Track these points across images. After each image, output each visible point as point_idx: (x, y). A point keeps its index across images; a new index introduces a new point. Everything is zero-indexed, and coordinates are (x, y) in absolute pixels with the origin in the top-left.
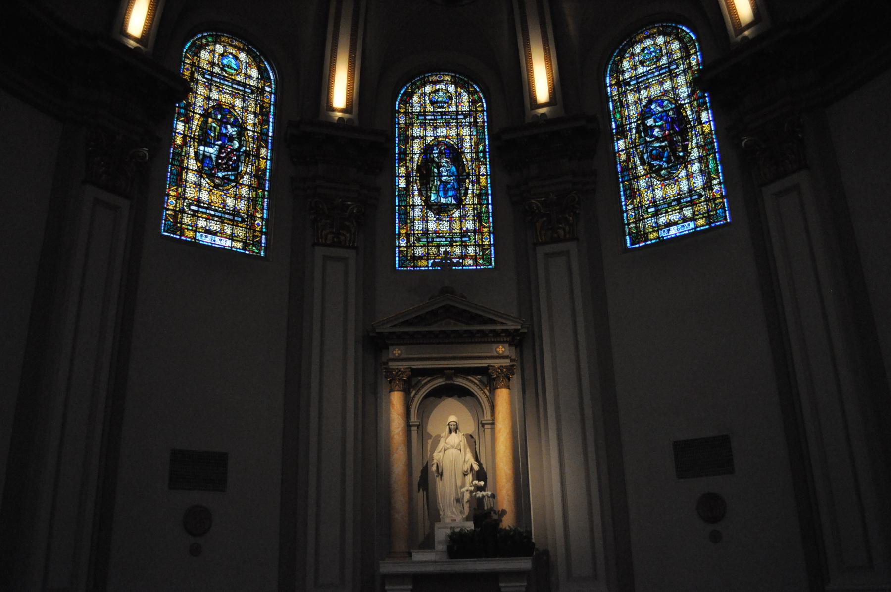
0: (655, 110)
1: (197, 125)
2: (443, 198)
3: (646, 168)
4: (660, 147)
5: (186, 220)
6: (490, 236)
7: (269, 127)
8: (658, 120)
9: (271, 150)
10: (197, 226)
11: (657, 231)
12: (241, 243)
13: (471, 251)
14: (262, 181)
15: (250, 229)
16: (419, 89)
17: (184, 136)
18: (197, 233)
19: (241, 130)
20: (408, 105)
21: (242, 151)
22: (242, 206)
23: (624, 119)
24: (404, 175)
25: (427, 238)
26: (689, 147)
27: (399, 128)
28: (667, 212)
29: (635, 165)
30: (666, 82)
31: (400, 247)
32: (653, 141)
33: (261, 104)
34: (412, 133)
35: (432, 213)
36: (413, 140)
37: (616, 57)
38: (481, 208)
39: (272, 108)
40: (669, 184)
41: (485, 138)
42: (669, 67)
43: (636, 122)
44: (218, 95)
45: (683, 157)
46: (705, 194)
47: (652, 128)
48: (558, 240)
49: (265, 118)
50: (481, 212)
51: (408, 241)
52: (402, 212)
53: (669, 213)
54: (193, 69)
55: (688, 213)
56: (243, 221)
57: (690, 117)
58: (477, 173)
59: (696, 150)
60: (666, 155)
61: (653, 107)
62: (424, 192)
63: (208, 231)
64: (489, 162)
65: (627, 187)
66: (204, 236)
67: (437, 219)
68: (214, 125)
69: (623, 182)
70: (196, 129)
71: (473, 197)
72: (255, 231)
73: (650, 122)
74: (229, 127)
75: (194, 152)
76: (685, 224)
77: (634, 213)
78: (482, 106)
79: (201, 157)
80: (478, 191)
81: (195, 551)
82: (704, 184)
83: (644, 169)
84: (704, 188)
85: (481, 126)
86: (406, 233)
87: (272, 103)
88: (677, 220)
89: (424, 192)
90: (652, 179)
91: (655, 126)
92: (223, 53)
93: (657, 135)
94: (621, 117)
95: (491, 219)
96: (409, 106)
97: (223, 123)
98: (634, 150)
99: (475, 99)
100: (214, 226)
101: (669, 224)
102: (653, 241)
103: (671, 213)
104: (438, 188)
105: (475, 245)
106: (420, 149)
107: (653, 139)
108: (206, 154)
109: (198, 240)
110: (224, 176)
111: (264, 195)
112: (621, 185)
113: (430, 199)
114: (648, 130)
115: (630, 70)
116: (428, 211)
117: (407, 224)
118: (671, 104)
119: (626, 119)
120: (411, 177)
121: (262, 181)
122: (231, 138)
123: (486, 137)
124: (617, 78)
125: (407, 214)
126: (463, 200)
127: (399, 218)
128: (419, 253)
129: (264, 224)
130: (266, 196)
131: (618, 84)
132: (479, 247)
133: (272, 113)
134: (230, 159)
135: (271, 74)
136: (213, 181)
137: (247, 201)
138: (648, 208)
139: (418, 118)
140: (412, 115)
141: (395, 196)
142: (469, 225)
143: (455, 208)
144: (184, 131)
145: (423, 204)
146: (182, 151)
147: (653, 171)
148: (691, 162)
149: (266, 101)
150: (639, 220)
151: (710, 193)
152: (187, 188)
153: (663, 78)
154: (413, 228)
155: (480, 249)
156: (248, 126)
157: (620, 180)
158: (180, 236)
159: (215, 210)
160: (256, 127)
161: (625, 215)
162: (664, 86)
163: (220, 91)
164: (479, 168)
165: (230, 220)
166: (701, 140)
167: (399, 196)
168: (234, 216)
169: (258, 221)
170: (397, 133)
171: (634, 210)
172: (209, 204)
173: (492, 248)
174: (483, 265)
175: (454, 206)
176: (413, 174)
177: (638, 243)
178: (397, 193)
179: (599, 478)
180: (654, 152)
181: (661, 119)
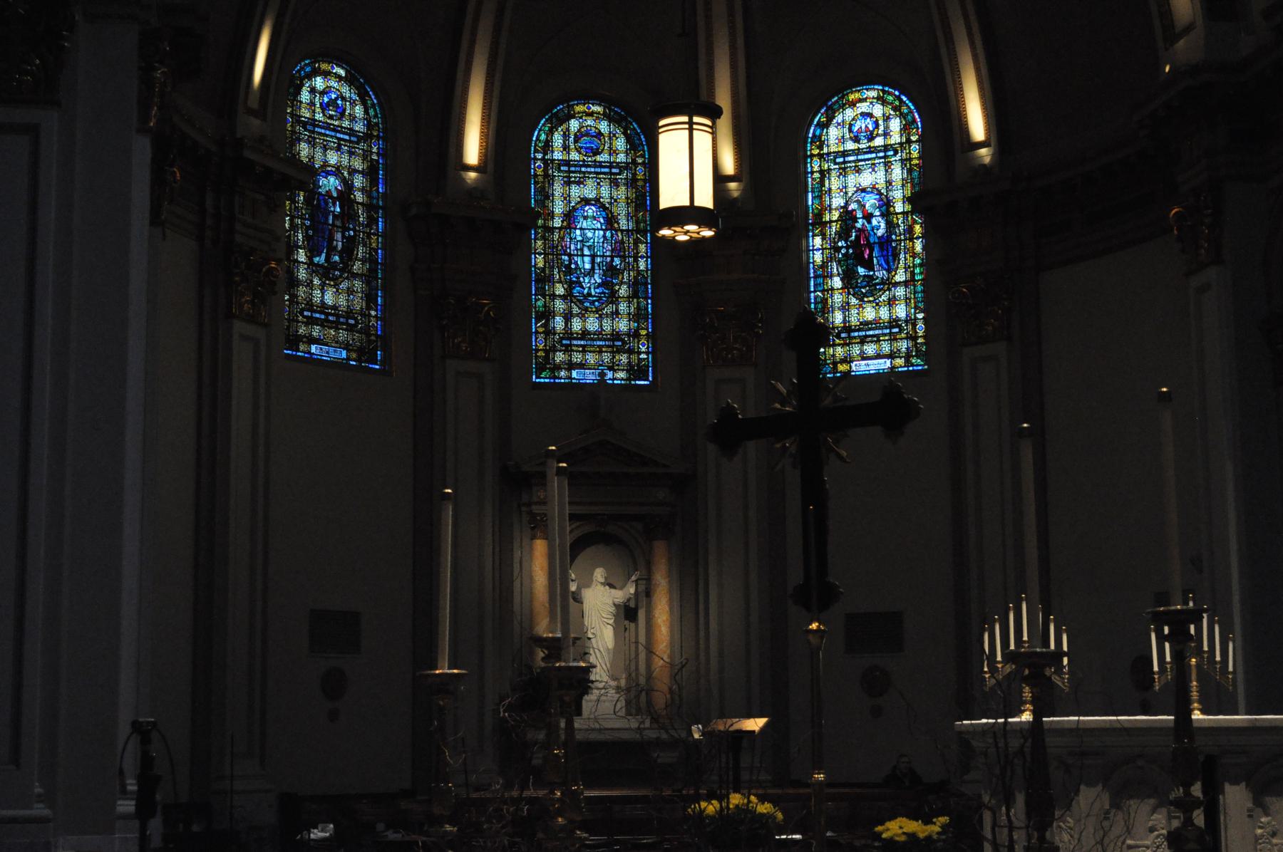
81: (334, 685)
165: (608, 346)
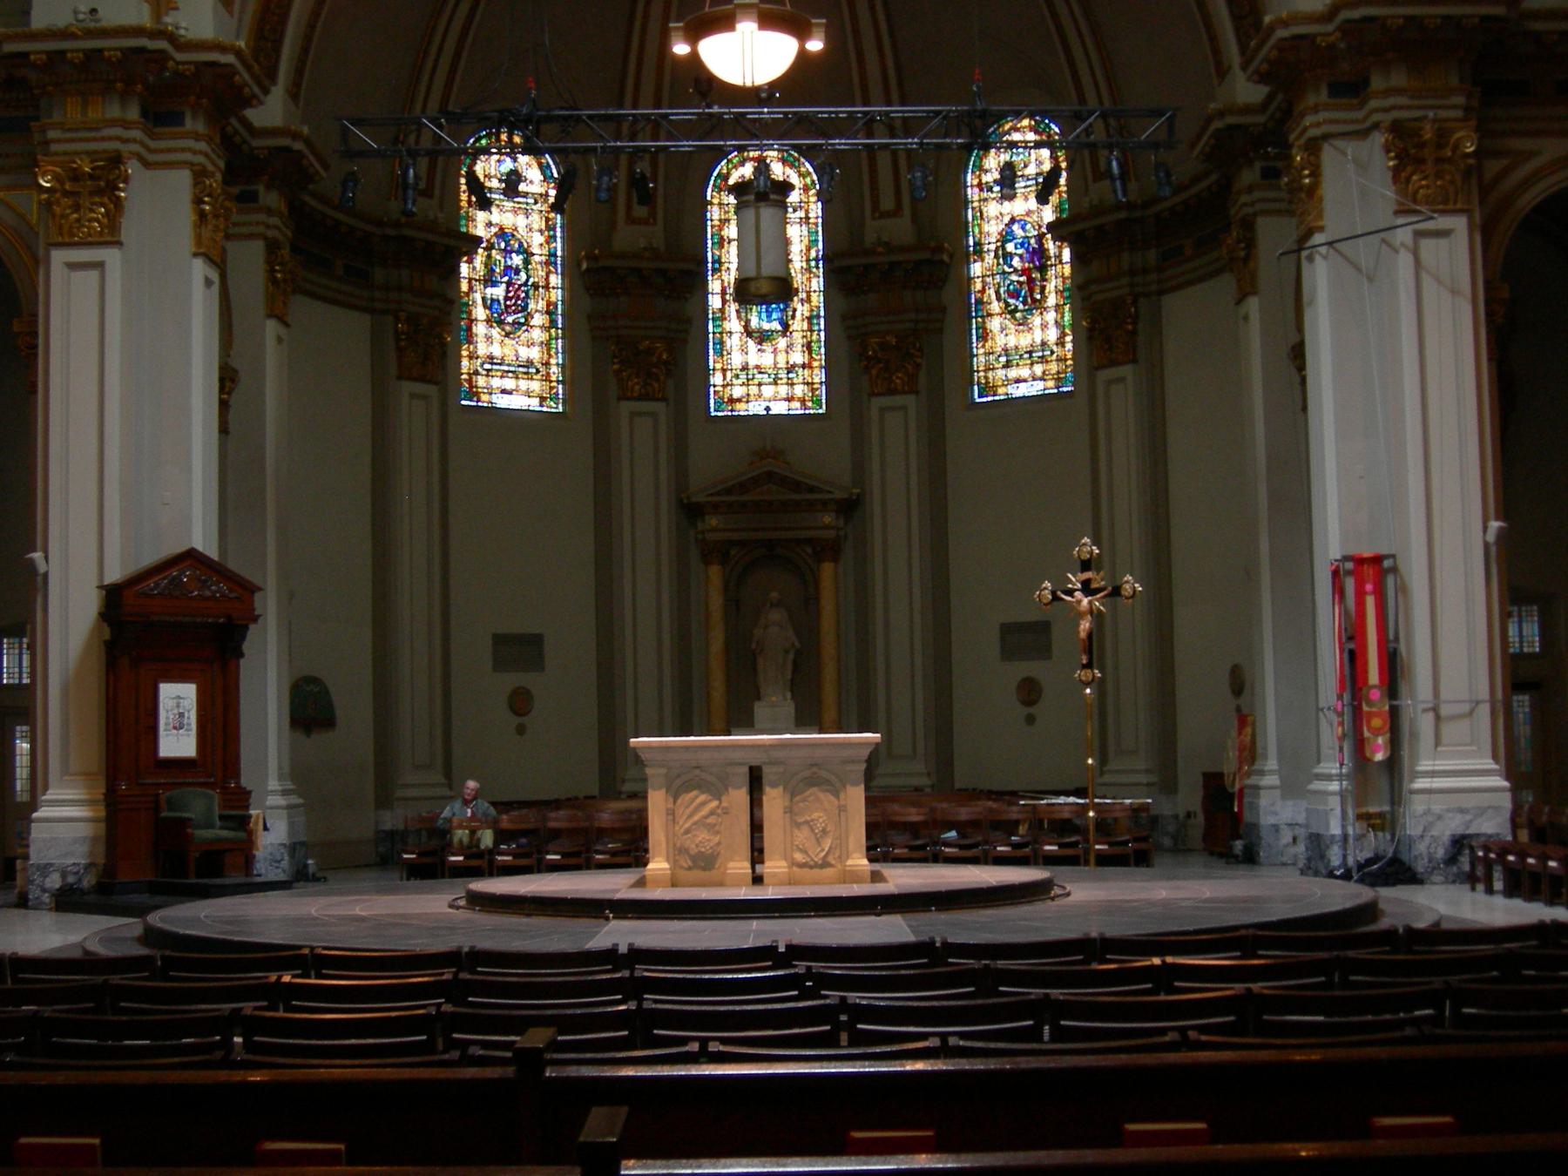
11: (1006, 385)
17: (470, 280)
28: (1018, 365)
32: (1011, 273)
36: (729, 243)
38: (811, 336)
45: (1039, 301)
47: (1011, 255)
48: (892, 392)
49: (552, 233)
52: (717, 341)
55: (1038, 369)
56: (538, 371)
62: (743, 315)
63: (504, 391)
69: (976, 317)
71: (803, 320)
79: (489, 302)
81: (521, 730)
89: (743, 315)
94: (980, 233)
97: (507, 252)
101: (1018, 381)
105: (804, 383)
114: (1008, 257)
117: (722, 356)
125: (722, 343)
131: (980, 185)
134: (518, 298)
136: (503, 330)
150: (990, 369)
157: (974, 314)
159: (509, 365)
161: (975, 359)
165: (525, 373)
172: (502, 359)
173: (824, 387)
179: (279, 757)
180: (1011, 287)
181: (1022, 245)
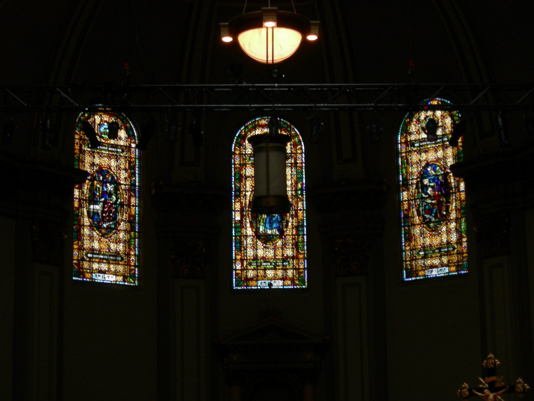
0: (430, 172)
1: (87, 189)
2: (269, 230)
3: (420, 219)
4: (431, 204)
5: (86, 265)
6: (304, 261)
7: (136, 179)
8: (431, 181)
9: (138, 198)
10: (92, 269)
11: (424, 270)
12: (122, 277)
13: (290, 273)
14: (133, 224)
15: (127, 265)
16: (251, 133)
17: (80, 200)
18: (93, 274)
19: (117, 185)
20: (242, 147)
21: (118, 203)
22: (121, 247)
23: (408, 174)
24: (239, 210)
25: (257, 263)
26: (450, 209)
27: (235, 168)
28: (432, 257)
29: (413, 215)
30: (440, 151)
31: (236, 270)
33: (129, 159)
34: (245, 173)
35: (260, 242)
36: (246, 179)
37: (406, 118)
38: (298, 238)
39: (137, 161)
40: (435, 235)
41: (303, 177)
42: (442, 138)
43: (416, 179)
44: (99, 160)
45: (445, 216)
46: (457, 248)
47: (427, 187)
50: (298, 242)
51: (242, 265)
53: (433, 258)
54: (81, 143)
55: (445, 260)
57: (453, 184)
58: (296, 208)
59: (454, 212)
60: (434, 211)
61: (429, 169)
62: (254, 224)
63: (101, 272)
64: (306, 198)
65: (407, 231)
66: (97, 275)
67: (265, 247)
68: (98, 186)
69: (404, 227)
70: (87, 192)
71: (293, 228)
72: (130, 266)
73: (426, 182)
74: (108, 185)
75: (87, 211)
76: (443, 268)
77: (410, 253)
78: (301, 149)
80: (296, 224)
82: (457, 240)
83: (419, 219)
84: (457, 243)
85: (300, 167)
86: (241, 259)
87: (137, 157)
88: (437, 264)
89: (254, 224)
90: (424, 229)
91: (430, 186)
92: (100, 122)
93: (430, 193)
94: (407, 172)
95: (305, 247)
96: (243, 148)
97: (104, 183)
98: (414, 202)
99: (296, 142)
100: (104, 267)
101: (432, 267)
102: (421, 278)
103: (434, 258)
104: (266, 221)
105: (293, 269)
106: (251, 187)
107: (427, 196)
108: (94, 211)
109: (95, 279)
110: (107, 226)
111: (135, 235)
112: (403, 228)
113: (259, 230)
115: (415, 133)
116: (257, 240)
118: (442, 170)
119: (410, 175)
120: (244, 211)
121: (133, 224)
122: (110, 194)
123: (304, 176)
124: (406, 137)
125: (241, 242)
126: (284, 231)
127: (235, 247)
128: (251, 275)
129: (136, 259)
130: (137, 236)
131: (406, 143)
132: (296, 270)
133: (137, 166)
134: (110, 212)
135: (135, 131)
137: (124, 243)
138: (420, 251)
139: (250, 159)
140: (245, 156)
141: (232, 227)
142: (289, 252)
143: (278, 238)
144: (79, 196)
145: (254, 235)
146: (79, 212)
147: (426, 223)
148: (450, 221)
149: (132, 157)
150: (413, 260)
151: (460, 248)
152: (84, 241)
153: (437, 147)
154: (246, 254)
155: (297, 272)
156: (121, 181)
158: (83, 278)
159: (104, 255)
160: (127, 180)
162: (438, 154)
163: (101, 156)
164: (298, 204)
166: (458, 204)
167: (235, 227)
168: (115, 256)
169: (133, 258)
170: (233, 172)
171: (411, 251)
172: (100, 251)
173: (306, 271)
174: (299, 285)
175: (278, 236)
176: (246, 209)
177: (411, 277)
178: (233, 225)
180: (427, 207)
181: (434, 180)
